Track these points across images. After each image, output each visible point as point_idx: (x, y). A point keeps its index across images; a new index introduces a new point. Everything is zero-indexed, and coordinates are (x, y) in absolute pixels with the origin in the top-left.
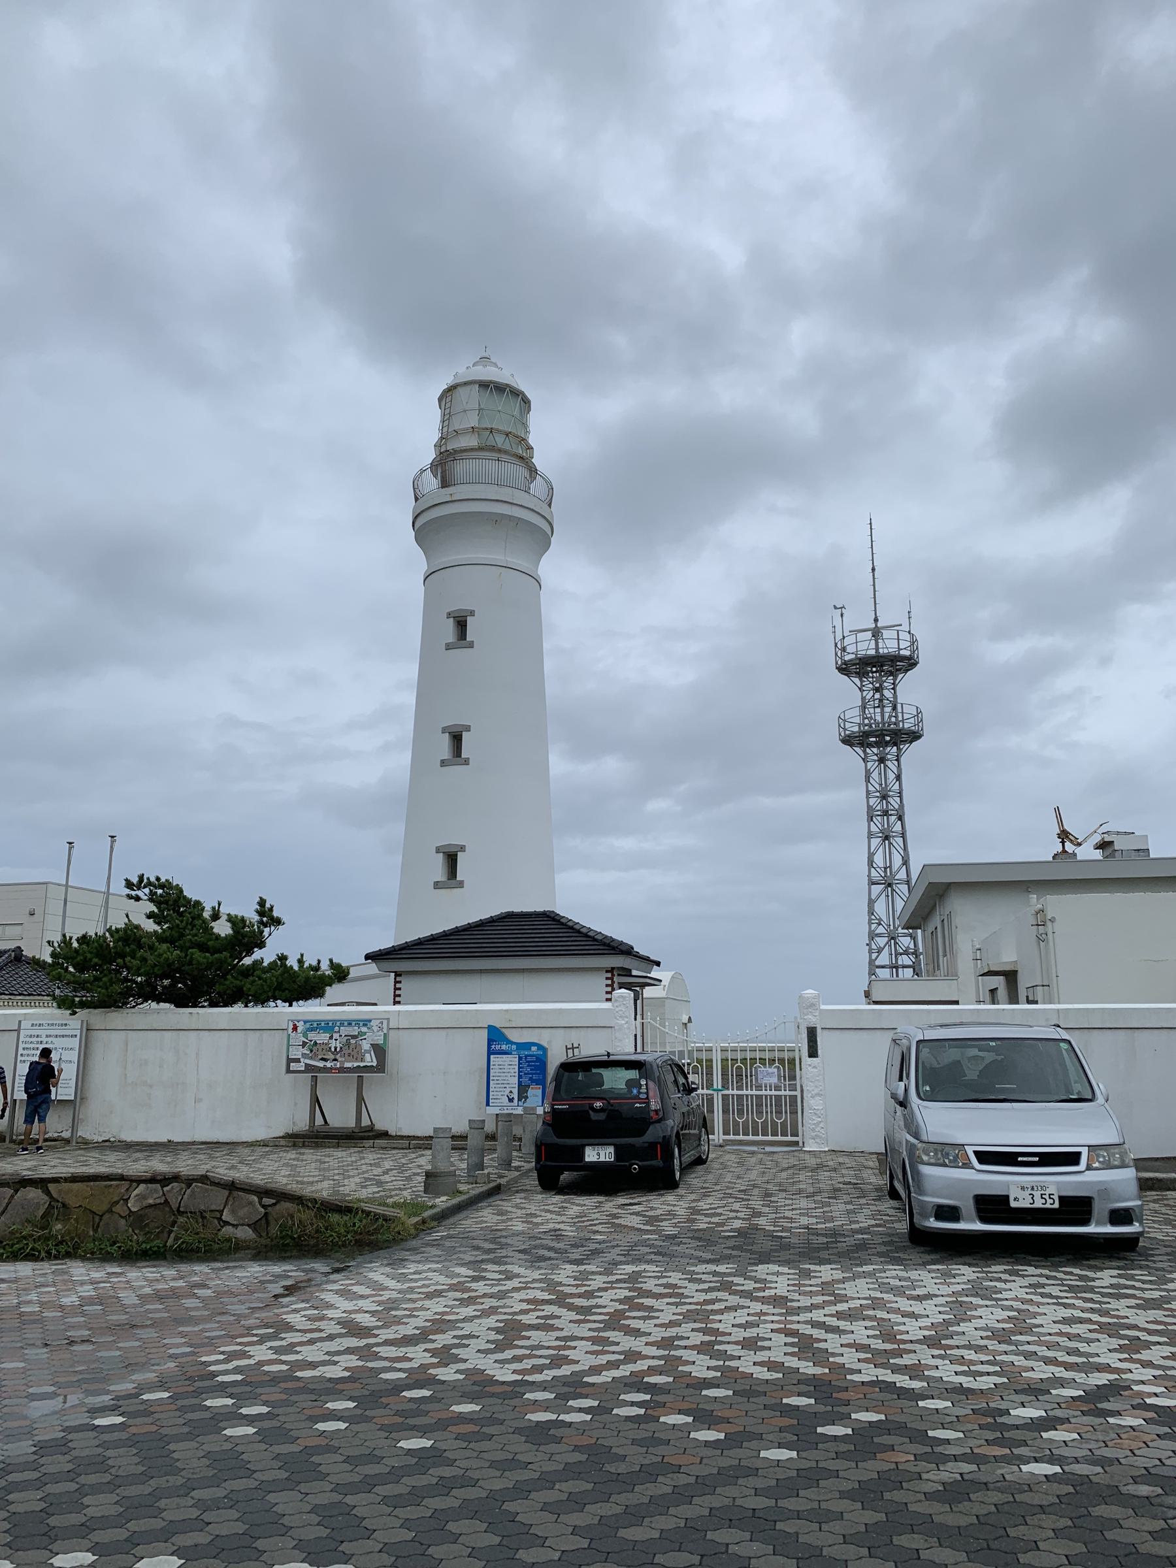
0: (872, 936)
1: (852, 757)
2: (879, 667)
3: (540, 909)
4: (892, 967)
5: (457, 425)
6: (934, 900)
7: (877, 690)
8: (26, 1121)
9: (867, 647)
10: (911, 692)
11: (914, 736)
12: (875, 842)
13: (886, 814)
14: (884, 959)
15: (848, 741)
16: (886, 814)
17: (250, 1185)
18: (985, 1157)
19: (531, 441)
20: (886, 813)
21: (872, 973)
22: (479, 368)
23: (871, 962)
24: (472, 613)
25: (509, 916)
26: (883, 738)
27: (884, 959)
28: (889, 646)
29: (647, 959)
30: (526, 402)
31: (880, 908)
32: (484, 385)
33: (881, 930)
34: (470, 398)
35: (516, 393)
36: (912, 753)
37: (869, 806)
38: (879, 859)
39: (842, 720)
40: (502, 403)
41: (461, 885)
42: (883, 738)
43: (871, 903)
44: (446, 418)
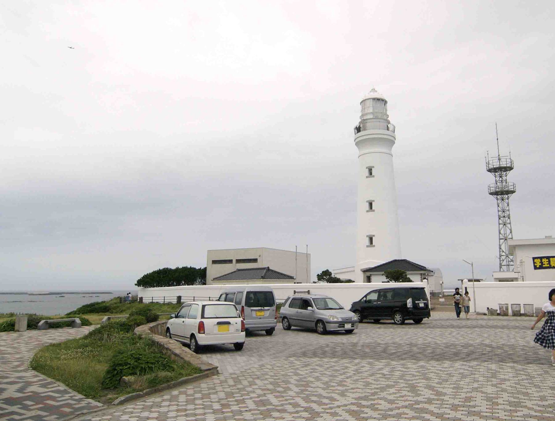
0: (501, 256)
1: (493, 198)
2: (500, 170)
3: (403, 258)
4: (507, 265)
5: (367, 111)
6: (513, 249)
7: (501, 177)
8: (358, 308)
9: (496, 165)
10: (510, 176)
11: (513, 192)
12: (501, 226)
13: (504, 218)
14: (504, 263)
15: (491, 194)
16: (504, 218)
17: (195, 381)
18: (238, 261)
19: (388, 113)
20: (504, 217)
21: (500, 268)
22: (372, 93)
23: (500, 264)
24: (373, 167)
25: (395, 261)
26: (502, 193)
27: (504, 263)
28: (503, 164)
29: (429, 271)
30: (385, 102)
31: (503, 247)
32: (374, 99)
33: (504, 254)
34: (370, 103)
35: (383, 100)
36: (512, 197)
37: (499, 215)
38: (502, 232)
39: (489, 187)
40: (379, 104)
41: (374, 246)
42: (502, 193)
43: (500, 245)
44: (363, 109)
